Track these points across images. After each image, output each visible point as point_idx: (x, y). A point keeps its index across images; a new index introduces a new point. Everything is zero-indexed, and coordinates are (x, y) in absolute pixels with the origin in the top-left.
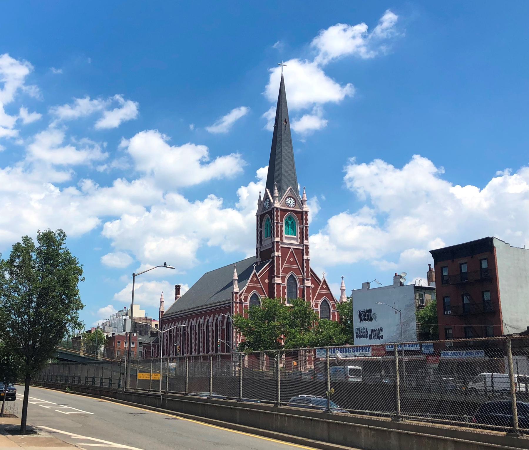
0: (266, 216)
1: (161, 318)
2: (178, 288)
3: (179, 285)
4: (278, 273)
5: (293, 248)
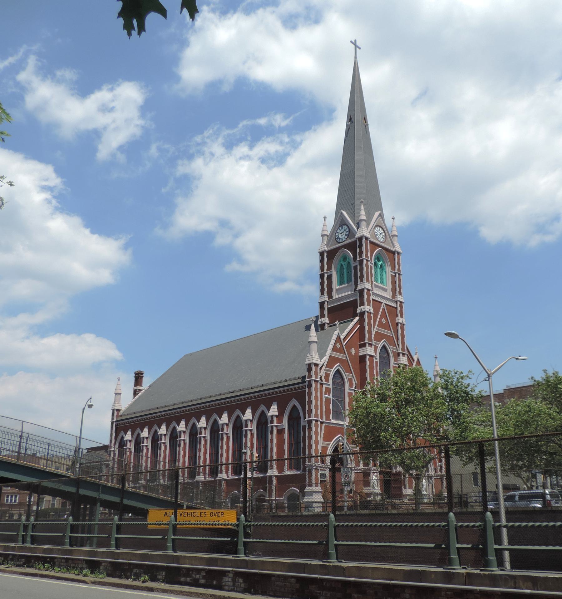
1: (116, 421)
2: (138, 378)
3: (141, 371)
4: (370, 339)
5: (385, 304)
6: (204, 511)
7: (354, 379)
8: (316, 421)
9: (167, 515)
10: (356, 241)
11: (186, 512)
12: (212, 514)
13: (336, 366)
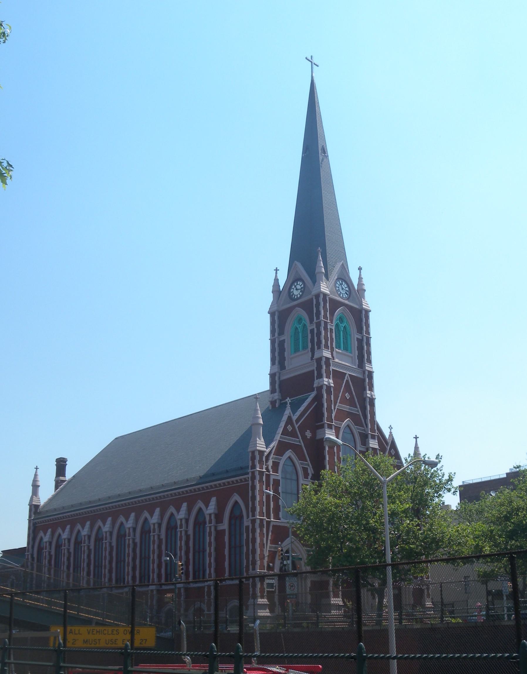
0: (294, 312)
4: (330, 419)
5: (349, 374)
6: (116, 629)
7: (310, 468)
8: (262, 520)
9: (72, 633)
10: (312, 300)
11: (94, 630)
12: (125, 632)
13: (289, 453)
